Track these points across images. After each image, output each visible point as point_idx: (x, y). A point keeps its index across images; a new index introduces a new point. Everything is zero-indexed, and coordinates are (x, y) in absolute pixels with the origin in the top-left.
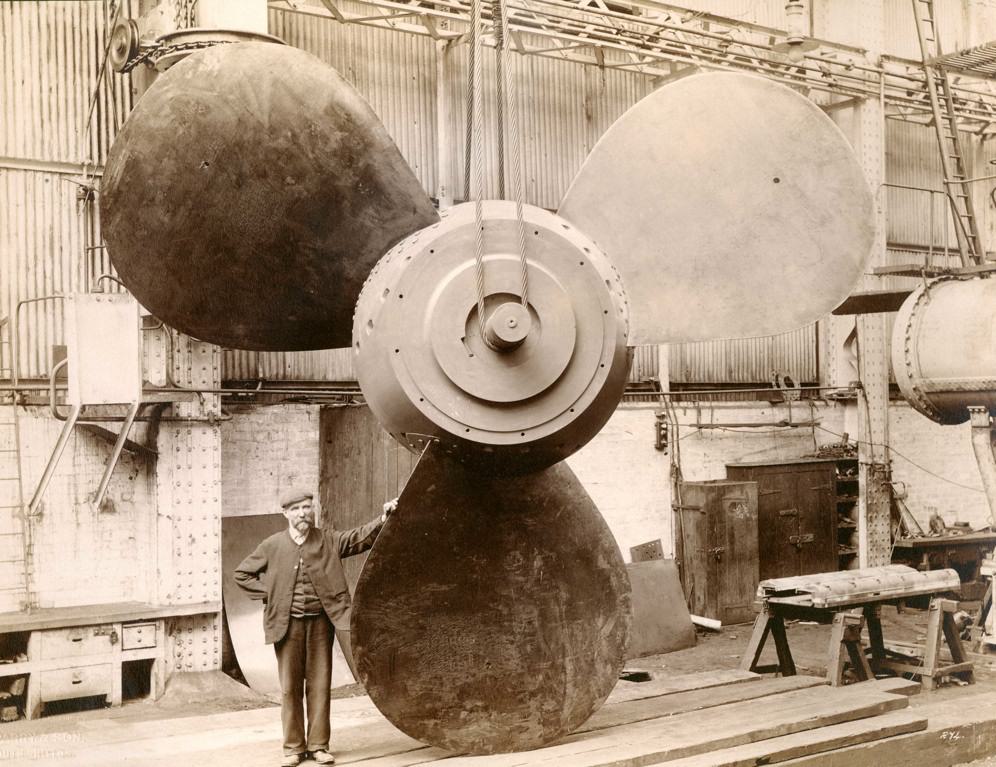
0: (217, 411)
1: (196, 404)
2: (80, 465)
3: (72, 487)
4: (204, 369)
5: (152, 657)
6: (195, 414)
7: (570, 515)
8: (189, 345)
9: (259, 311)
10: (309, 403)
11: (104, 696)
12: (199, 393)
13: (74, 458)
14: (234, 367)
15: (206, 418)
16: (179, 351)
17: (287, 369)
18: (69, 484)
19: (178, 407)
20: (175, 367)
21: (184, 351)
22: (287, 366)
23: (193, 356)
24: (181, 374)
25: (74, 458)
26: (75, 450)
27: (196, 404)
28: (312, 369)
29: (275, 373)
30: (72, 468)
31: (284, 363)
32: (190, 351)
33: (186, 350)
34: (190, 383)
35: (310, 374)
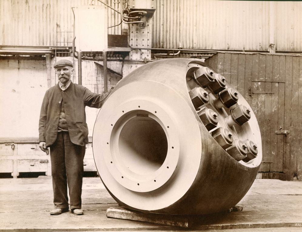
0: (149, 58)
1: (139, 54)
2: (99, 81)
3: (96, 89)
4: (143, 40)
5: (20, 179)
6: (139, 59)
7: (55, 162)
8: (137, 30)
9: (271, 77)
10: (201, 58)
11: (256, 148)
12: (140, 49)
13: (97, 78)
14: (170, 44)
15: (143, 60)
16: (132, 32)
17: (194, 44)
18: (95, 88)
19: (132, 56)
20: (130, 39)
21: (135, 32)
22: (194, 43)
23: (139, 34)
24: (133, 42)
25: (97, 78)
26: (97, 75)
27: (139, 54)
28: (206, 44)
29: (188, 46)
30: (96, 81)
31: (193, 42)
32: (137, 33)
33: (136, 32)
34: (137, 46)
35: (205, 47)
